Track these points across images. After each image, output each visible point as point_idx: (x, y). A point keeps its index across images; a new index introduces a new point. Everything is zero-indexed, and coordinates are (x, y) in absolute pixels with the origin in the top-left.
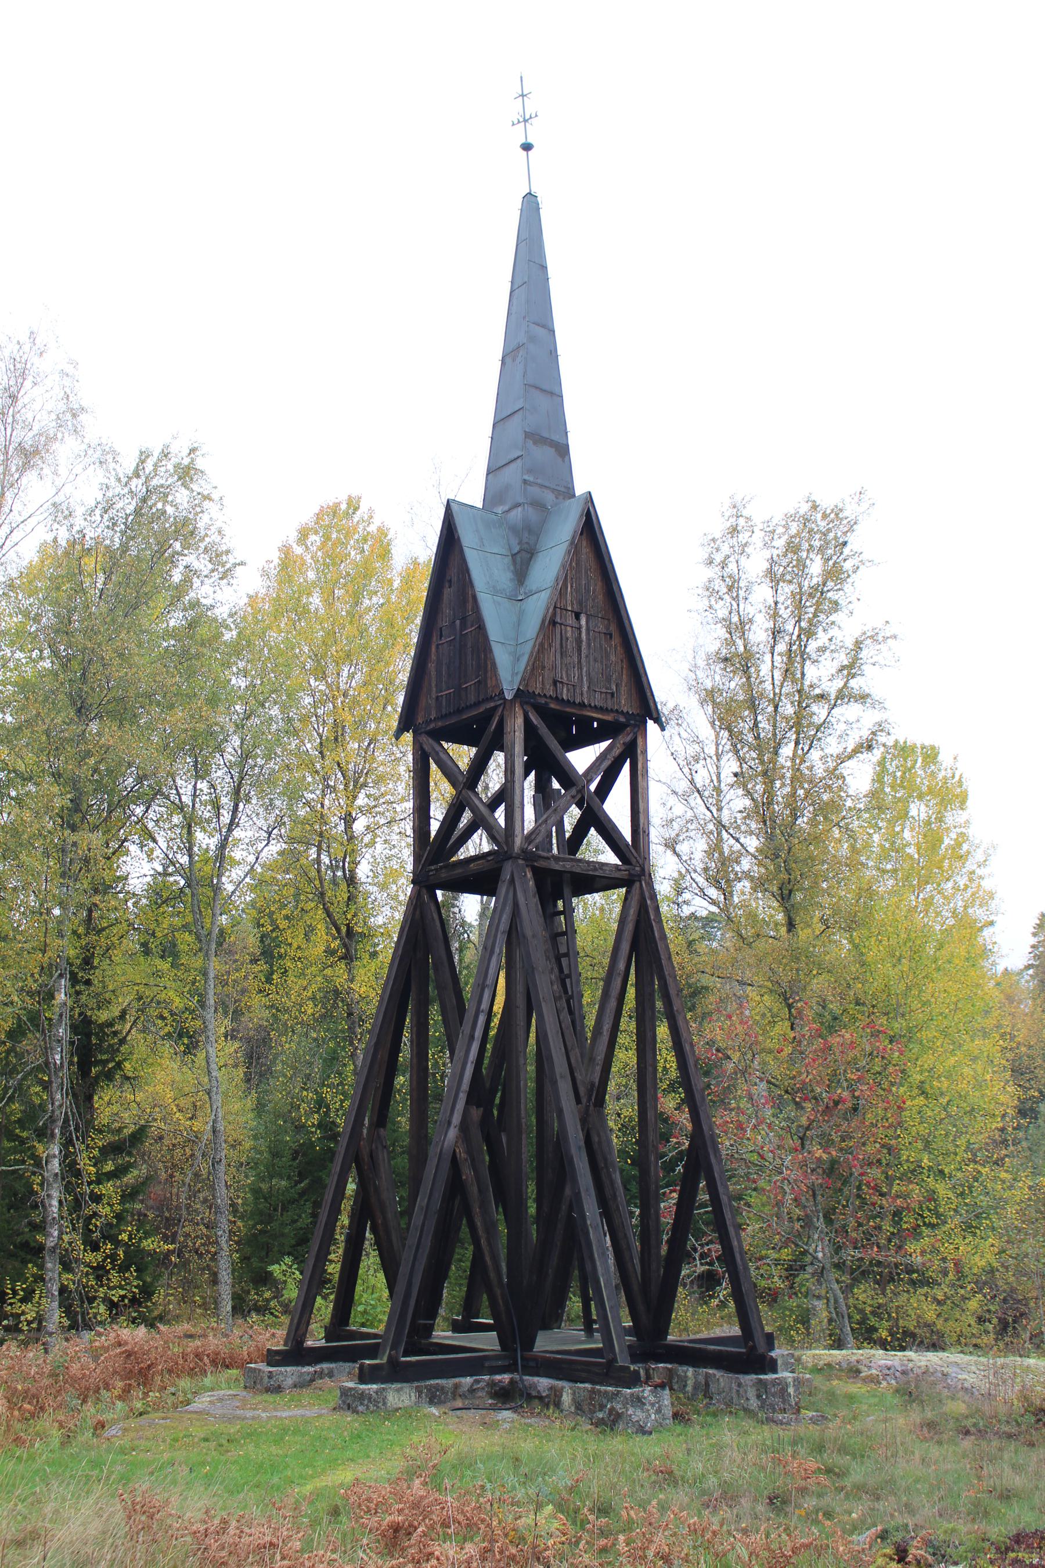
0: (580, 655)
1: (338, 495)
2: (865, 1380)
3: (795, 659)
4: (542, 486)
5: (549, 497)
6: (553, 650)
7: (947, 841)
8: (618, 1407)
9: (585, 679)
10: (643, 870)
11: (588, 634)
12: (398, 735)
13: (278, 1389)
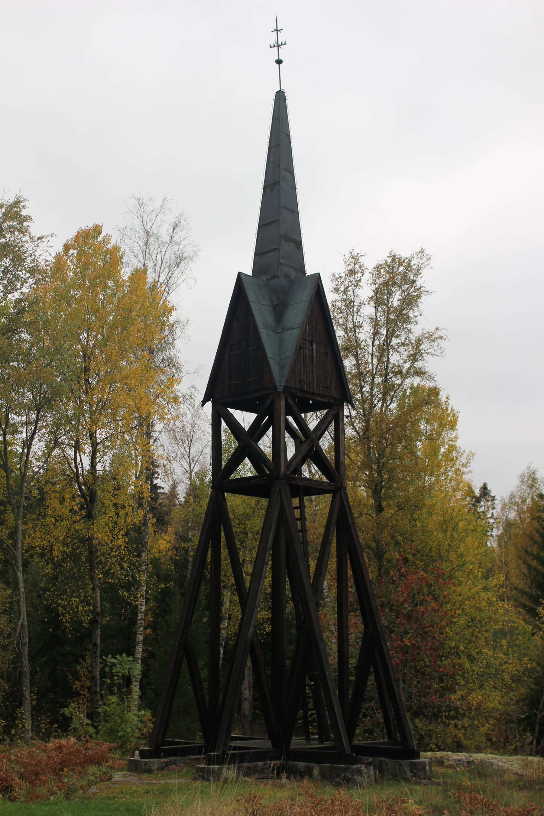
0: (313, 365)
1: (88, 224)
2: (447, 767)
3: (384, 349)
4: (289, 266)
5: (293, 273)
6: (299, 363)
7: (442, 450)
8: (349, 775)
9: (315, 379)
10: (342, 485)
11: (316, 353)
12: (203, 403)
13: (150, 771)
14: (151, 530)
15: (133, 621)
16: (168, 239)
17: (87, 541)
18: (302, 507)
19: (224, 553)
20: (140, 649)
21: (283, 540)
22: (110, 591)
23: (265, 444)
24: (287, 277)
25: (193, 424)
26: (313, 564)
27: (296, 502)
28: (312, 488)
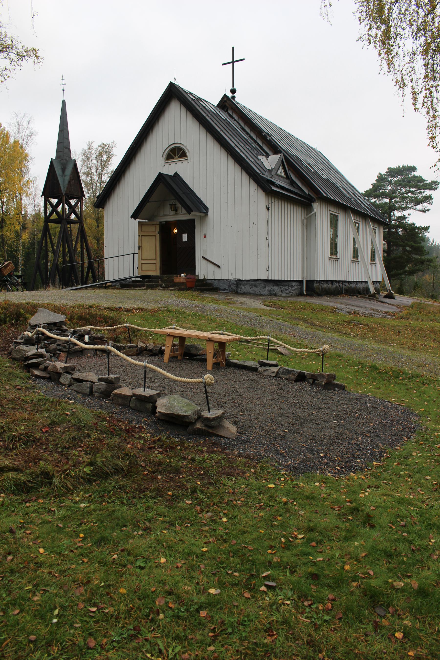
5: (68, 158)
16: (26, 127)
18: (70, 227)
19: (48, 240)
21: (65, 237)
23: (60, 209)
24: (66, 160)
25: (35, 192)
26: (74, 243)
27: (69, 226)
28: (73, 222)
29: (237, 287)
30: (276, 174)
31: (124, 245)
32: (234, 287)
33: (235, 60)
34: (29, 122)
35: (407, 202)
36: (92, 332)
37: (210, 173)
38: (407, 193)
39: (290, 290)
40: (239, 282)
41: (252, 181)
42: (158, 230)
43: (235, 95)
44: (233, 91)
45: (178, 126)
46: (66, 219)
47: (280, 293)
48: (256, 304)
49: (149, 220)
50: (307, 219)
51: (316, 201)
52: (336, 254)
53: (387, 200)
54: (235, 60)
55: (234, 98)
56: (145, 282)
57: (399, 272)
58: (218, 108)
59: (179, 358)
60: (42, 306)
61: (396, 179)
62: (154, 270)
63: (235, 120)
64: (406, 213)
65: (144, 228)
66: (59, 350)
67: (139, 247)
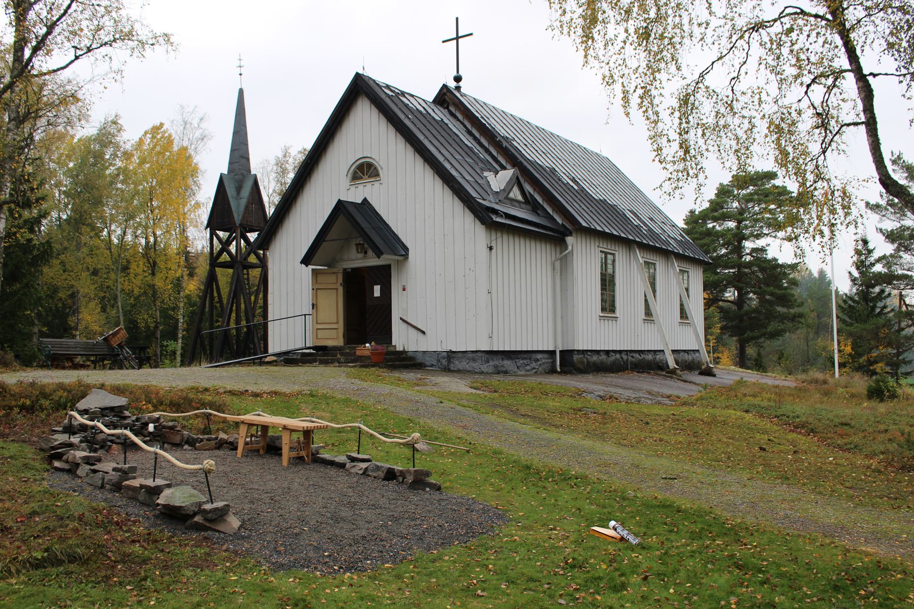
5: (245, 172)
14: (186, 278)
15: (176, 327)
17: (152, 287)
18: (248, 274)
20: (180, 341)
22: (164, 312)
23: (233, 248)
27: (245, 271)
28: (253, 266)
29: (448, 362)
30: (507, 198)
31: (295, 302)
32: (444, 362)
33: (460, 35)
34: (201, 119)
35: (762, 227)
36: (162, 420)
37: (409, 199)
38: (761, 213)
39: (534, 365)
40: (451, 355)
41: (467, 210)
42: (340, 280)
43: (461, 84)
44: (458, 79)
45: (367, 132)
46: (241, 262)
47: (516, 369)
48: (458, 385)
49: (329, 265)
50: (561, 259)
51: (574, 235)
52: (612, 309)
53: (732, 224)
54: (460, 35)
55: (458, 88)
56: (320, 355)
57: (756, 333)
58: (433, 106)
59: (261, 452)
60: (95, 386)
61: (744, 192)
62: (335, 338)
63: (459, 120)
64: (760, 243)
65: (321, 278)
66: (112, 441)
67: (313, 305)
